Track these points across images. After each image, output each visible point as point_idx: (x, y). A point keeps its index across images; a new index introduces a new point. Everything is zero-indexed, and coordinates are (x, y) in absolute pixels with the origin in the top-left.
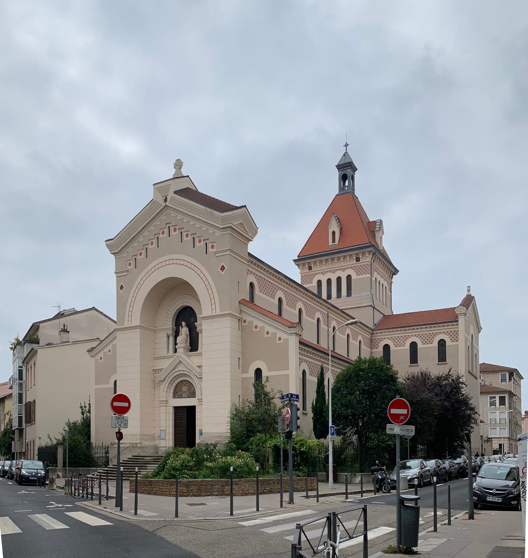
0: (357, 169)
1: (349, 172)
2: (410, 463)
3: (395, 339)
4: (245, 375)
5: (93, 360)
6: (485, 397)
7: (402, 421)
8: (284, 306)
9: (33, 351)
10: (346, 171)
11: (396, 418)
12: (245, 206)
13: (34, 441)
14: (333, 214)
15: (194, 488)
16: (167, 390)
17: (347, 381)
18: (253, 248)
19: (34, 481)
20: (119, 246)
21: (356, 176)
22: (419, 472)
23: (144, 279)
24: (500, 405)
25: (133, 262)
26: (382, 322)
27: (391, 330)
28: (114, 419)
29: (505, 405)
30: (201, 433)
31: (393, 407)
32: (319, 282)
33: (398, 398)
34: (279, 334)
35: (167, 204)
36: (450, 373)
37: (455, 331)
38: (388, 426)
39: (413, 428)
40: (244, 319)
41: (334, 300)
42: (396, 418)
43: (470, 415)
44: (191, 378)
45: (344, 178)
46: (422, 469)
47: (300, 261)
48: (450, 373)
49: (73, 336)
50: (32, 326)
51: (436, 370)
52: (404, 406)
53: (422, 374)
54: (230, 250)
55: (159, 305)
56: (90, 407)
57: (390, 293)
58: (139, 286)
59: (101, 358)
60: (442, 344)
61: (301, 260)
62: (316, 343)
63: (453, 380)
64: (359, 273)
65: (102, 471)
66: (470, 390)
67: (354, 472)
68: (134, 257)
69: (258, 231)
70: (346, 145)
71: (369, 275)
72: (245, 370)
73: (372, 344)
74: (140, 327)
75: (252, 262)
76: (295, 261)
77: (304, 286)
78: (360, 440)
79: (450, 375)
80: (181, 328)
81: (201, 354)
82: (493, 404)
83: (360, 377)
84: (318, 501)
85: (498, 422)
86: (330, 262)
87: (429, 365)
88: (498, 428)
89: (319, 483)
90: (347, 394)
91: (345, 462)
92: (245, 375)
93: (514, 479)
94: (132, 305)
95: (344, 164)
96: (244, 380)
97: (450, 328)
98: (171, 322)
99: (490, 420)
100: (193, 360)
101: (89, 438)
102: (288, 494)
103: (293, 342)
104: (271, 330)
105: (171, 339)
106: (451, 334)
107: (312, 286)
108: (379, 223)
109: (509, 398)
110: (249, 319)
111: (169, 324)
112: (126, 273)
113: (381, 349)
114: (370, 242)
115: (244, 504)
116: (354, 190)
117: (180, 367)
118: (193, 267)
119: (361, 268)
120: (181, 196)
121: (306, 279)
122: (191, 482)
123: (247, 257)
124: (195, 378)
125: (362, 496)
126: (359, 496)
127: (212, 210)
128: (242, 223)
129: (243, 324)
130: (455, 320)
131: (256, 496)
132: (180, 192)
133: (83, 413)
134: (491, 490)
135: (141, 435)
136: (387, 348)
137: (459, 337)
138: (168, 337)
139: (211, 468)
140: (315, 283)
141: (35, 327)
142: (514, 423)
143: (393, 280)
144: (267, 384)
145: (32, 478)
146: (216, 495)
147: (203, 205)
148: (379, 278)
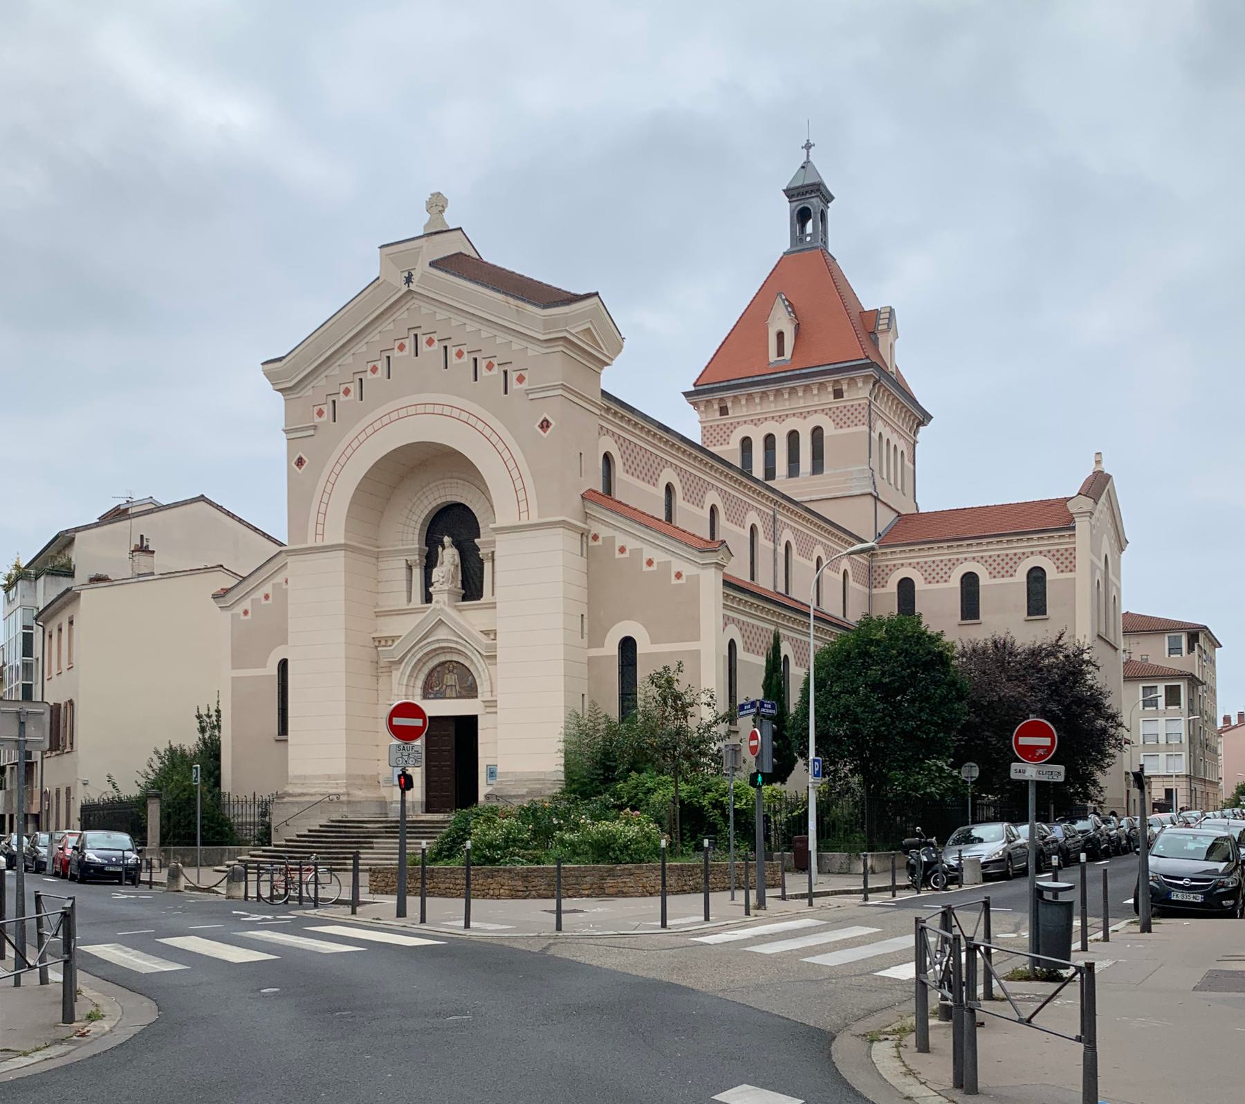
0: (833, 198)
1: (814, 203)
2: (978, 831)
3: (926, 567)
4: (594, 652)
5: (227, 615)
6: (1130, 685)
7: (1041, 757)
8: (679, 501)
9: (69, 594)
10: (808, 202)
11: (1030, 753)
12: (597, 294)
13: (68, 790)
14: (779, 294)
15: (541, 883)
16: (409, 680)
17: (839, 666)
18: (613, 380)
19: (116, 875)
20: (294, 376)
21: (830, 213)
22: (1004, 850)
23: (354, 445)
24: (1167, 705)
25: (327, 409)
26: (892, 530)
27: (916, 547)
28: (394, 750)
29: (1179, 704)
30: (492, 773)
31: (1023, 733)
32: (746, 443)
33: (1032, 718)
34: (677, 565)
35: (412, 287)
36: (1061, 643)
37: (1067, 550)
38: (1014, 766)
39: (1061, 768)
40: (593, 532)
41: (781, 481)
42: (941, 738)
43: (1104, 731)
44: (467, 657)
45: (803, 216)
46: (1010, 842)
47: (699, 394)
48: (1061, 643)
49: (161, 562)
50: (57, 537)
51: (1027, 635)
52: (1044, 732)
53: (995, 642)
54: (564, 387)
55: (388, 499)
56: (219, 716)
57: (911, 466)
58: (344, 458)
59: (246, 613)
60: (1036, 577)
61: (702, 393)
62: (748, 579)
63: (1067, 657)
64: (841, 423)
65: (260, 853)
66: (1105, 676)
67: (853, 850)
68: (331, 399)
69: (625, 344)
70: (808, 146)
71: (866, 428)
72: (596, 639)
73: (872, 577)
74: (345, 547)
75: (608, 409)
76: (687, 394)
77: (711, 449)
78: (865, 783)
79: (1060, 646)
80: (440, 549)
81: (493, 606)
82: (1150, 703)
83: (871, 657)
84: (811, 904)
85: (1162, 741)
86: (772, 398)
87: (1005, 621)
88: (1163, 755)
89: (786, 875)
90: (841, 692)
91: (834, 830)
92: (594, 652)
93: (1226, 859)
94: (325, 500)
95: (803, 187)
96: (592, 662)
97: (1056, 543)
98: (416, 537)
99: (1150, 737)
100: (472, 618)
101: (218, 783)
102: (743, 892)
103: (710, 583)
104: (631, 544)
105: (417, 573)
106: (1058, 555)
107: (730, 450)
108: (887, 315)
109: (1185, 690)
110: (604, 532)
111: (411, 541)
112: (311, 432)
113: (892, 587)
114: (868, 357)
115: (685, 910)
116: (825, 243)
117: (442, 634)
118: (472, 420)
119: (845, 411)
120: (447, 272)
121: (715, 434)
122: (535, 870)
123: (599, 399)
124: (475, 658)
125: (894, 896)
126: (887, 896)
127: (520, 303)
128: (588, 330)
129: (592, 543)
130: (1068, 526)
131: (660, 898)
132: (445, 264)
133: (203, 730)
134: (1181, 879)
135: (349, 777)
136: (906, 587)
137: (1077, 562)
138: (410, 568)
139: (572, 844)
140: (735, 444)
141: (64, 541)
142: (1201, 745)
143: (919, 437)
144: (679, 676)
145: (111, 869)
146: (588, 896)
147: (499, 291)
148: (887, 433)
